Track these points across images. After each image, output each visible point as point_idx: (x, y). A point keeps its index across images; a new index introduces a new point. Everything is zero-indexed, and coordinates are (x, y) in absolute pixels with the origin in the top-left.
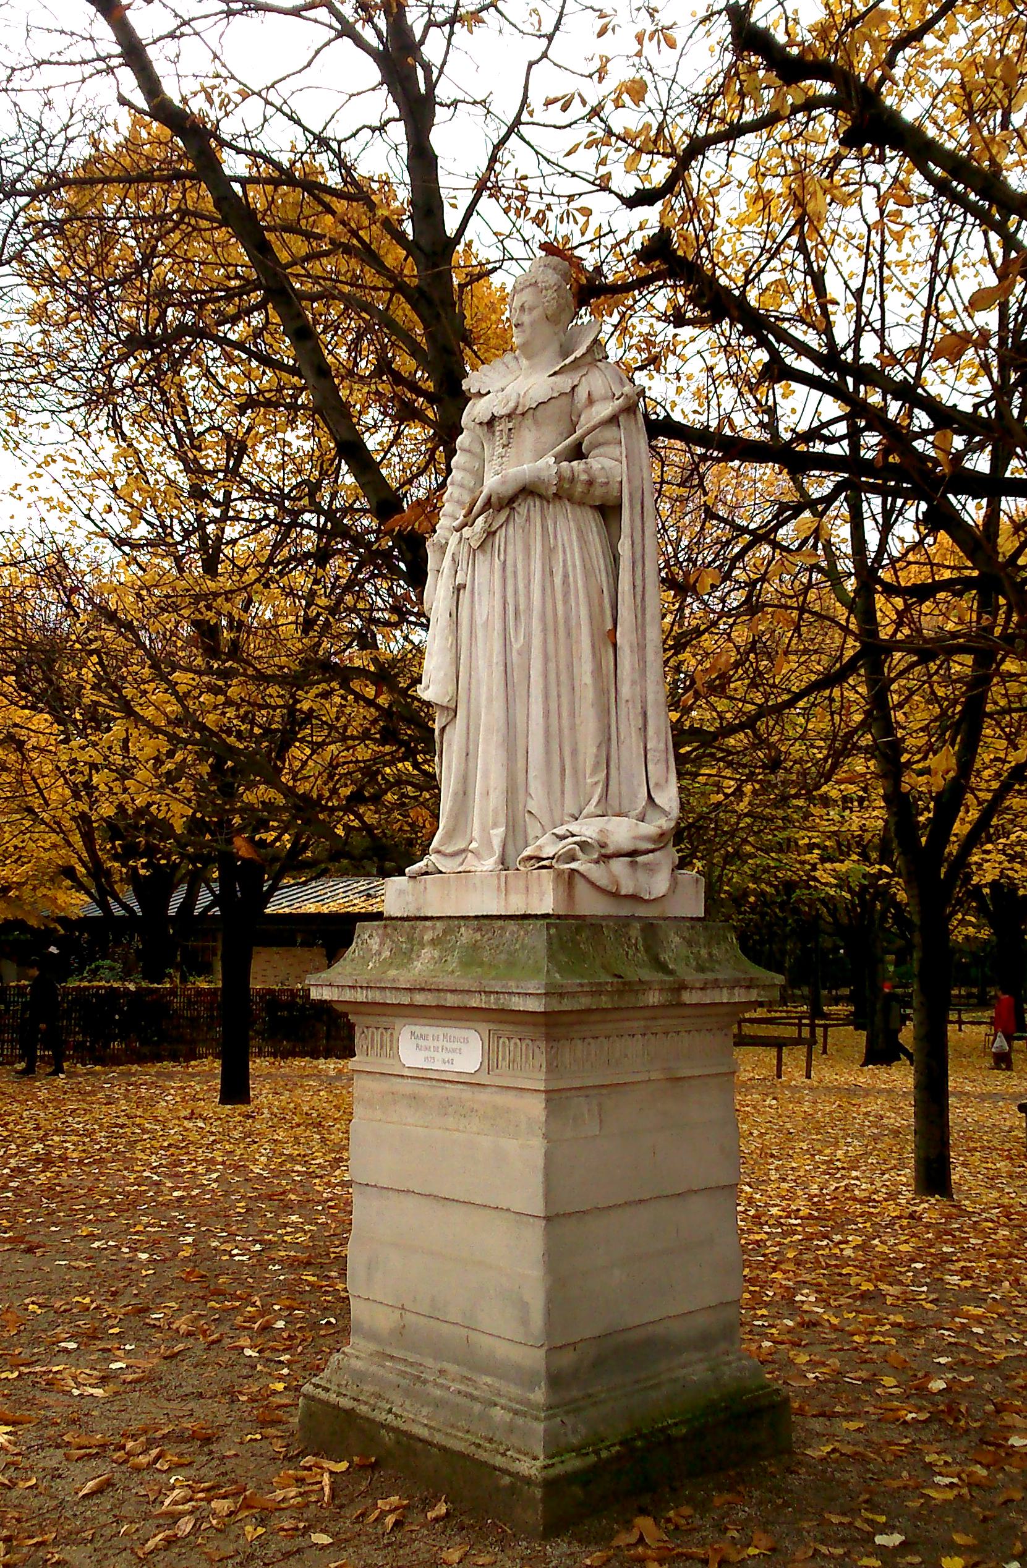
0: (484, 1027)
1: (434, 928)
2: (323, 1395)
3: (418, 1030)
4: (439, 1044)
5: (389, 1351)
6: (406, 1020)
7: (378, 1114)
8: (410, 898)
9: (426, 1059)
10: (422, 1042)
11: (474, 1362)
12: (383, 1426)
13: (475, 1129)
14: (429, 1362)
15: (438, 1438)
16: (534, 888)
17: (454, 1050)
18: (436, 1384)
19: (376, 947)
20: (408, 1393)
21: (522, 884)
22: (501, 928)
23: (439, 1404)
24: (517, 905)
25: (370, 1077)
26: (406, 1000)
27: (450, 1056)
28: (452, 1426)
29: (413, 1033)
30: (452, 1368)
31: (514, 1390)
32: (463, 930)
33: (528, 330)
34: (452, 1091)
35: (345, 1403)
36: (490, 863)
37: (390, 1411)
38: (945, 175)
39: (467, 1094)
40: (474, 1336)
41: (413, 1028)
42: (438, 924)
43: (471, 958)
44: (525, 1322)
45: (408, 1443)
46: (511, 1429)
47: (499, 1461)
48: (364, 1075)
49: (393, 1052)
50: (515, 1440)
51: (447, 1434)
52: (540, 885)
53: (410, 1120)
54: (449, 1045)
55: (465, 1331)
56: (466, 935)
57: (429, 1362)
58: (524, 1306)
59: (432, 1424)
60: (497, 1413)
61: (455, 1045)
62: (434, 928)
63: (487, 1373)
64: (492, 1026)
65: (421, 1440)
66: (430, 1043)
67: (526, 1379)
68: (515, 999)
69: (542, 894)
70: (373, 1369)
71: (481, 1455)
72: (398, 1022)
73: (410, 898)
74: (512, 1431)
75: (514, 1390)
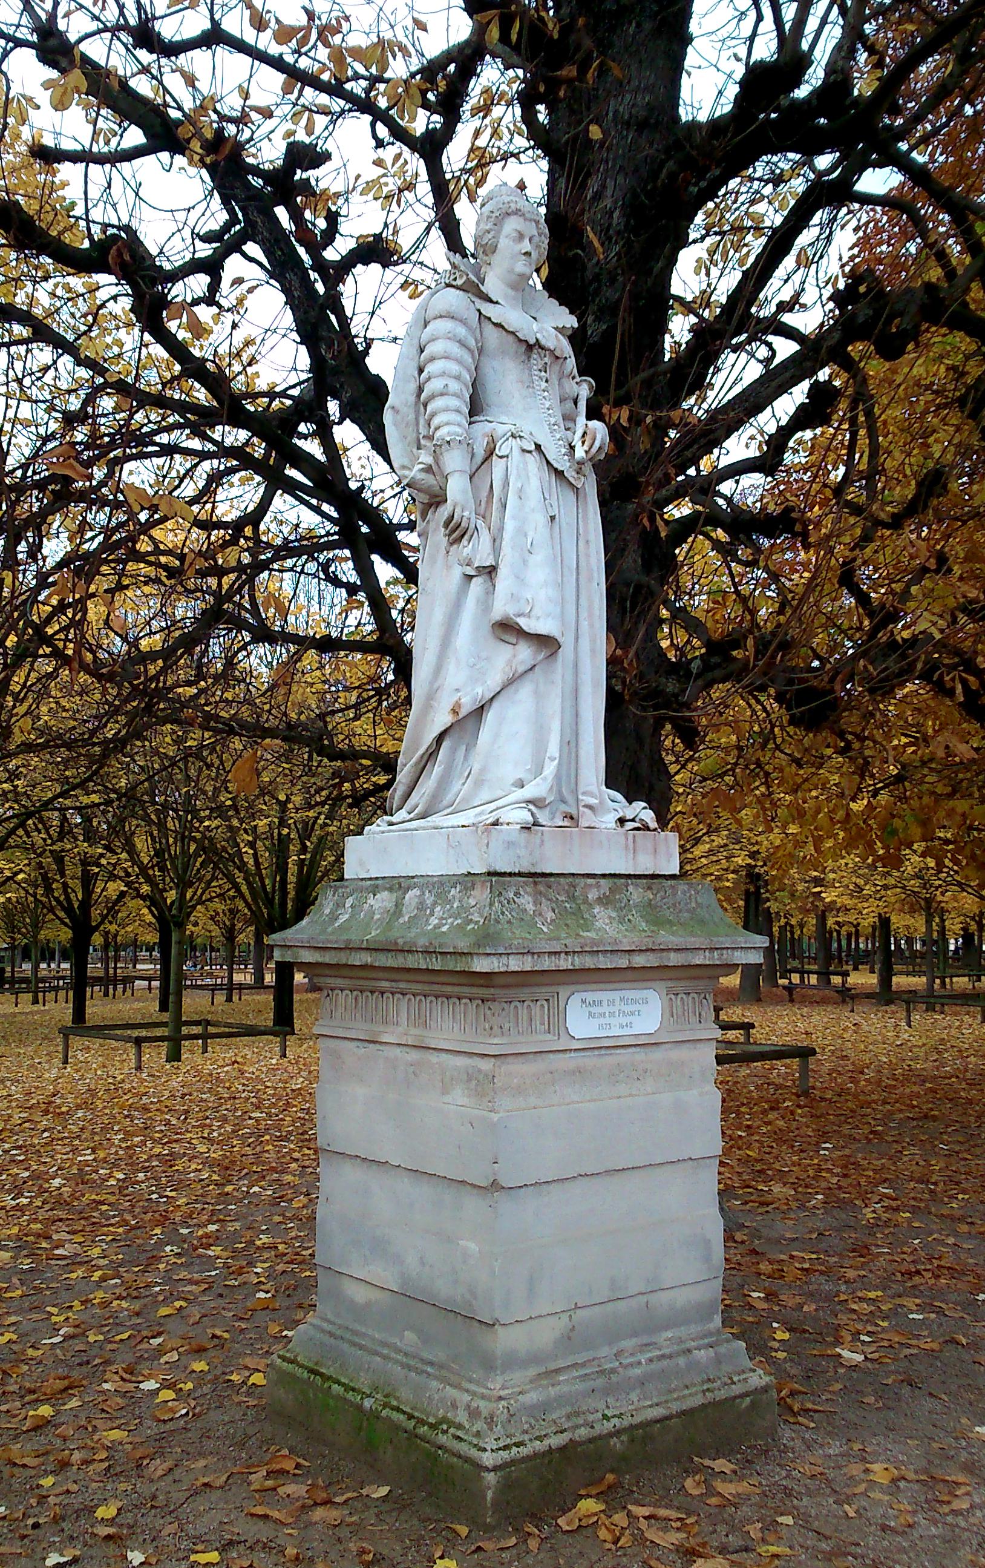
0: (662, 986)
1: (598, 886)
2: (524, 1451)
3: (590, 996)
4: (615, 1009)
5: (552, 1366)
6: (573, 988)
7: (533, 1101)
8: (522, 852)
9: (601, 1026)
10: (593, 1010)
11: (650, 1324)
12: (611, 1435)
13: (649, 1090)
14: (605, 1351)
15: (675, 1407)
16: (662, 849)
17: (632, 1013)
18: (626, 1367)
19: (530, 907)
20: (607, 1391)
21: (650, 845)
22: (672, 887)
23: (642, 1383)
24: (645, 865)
25: (521, 1059)
26: (623, 962)
27: (629, 1019)
28: (670, 1392)
29: (583, 1001)
30: (628, 1344)
31: (694, 1329)
32: (631, 888)
34: (623, 1056)
35: (556, 1441)
37: (605, 1417)
38: (805, 385)
39: (639, 1055)
40: (653, 1298)
41: (584, 995)
42: (602, 881)
43: (653, 914)
44: (707, 1259)
45: (642, 1435)
46: (718, 1360)
47: (737, 1390)
48: (510, 1059)
49: (557, 1023)
50: (726, 1368)
51: (676, 1399)
52: (668, 847)
53: (576, 1098)
54: (628, 1009)
55: (643, 1299)
56: (636, 893)
57: (605, 1351)
58: (707, 1242)
59: (655, 1400)
60: (702, 1355)
61: (637, 1007)
62: (598, 886)
63: (667, 1328)
64: (670, 984)
65: (658, 1421)
66: (605, 1009)
67: (702, 1312)
68: (737, 954)
69: (670, 855)
70: (552, 1391)
71: (722, 1394)
72: (564, 992)
73: (522, 852)
74: (720, 1362)
75: (694, 1329)
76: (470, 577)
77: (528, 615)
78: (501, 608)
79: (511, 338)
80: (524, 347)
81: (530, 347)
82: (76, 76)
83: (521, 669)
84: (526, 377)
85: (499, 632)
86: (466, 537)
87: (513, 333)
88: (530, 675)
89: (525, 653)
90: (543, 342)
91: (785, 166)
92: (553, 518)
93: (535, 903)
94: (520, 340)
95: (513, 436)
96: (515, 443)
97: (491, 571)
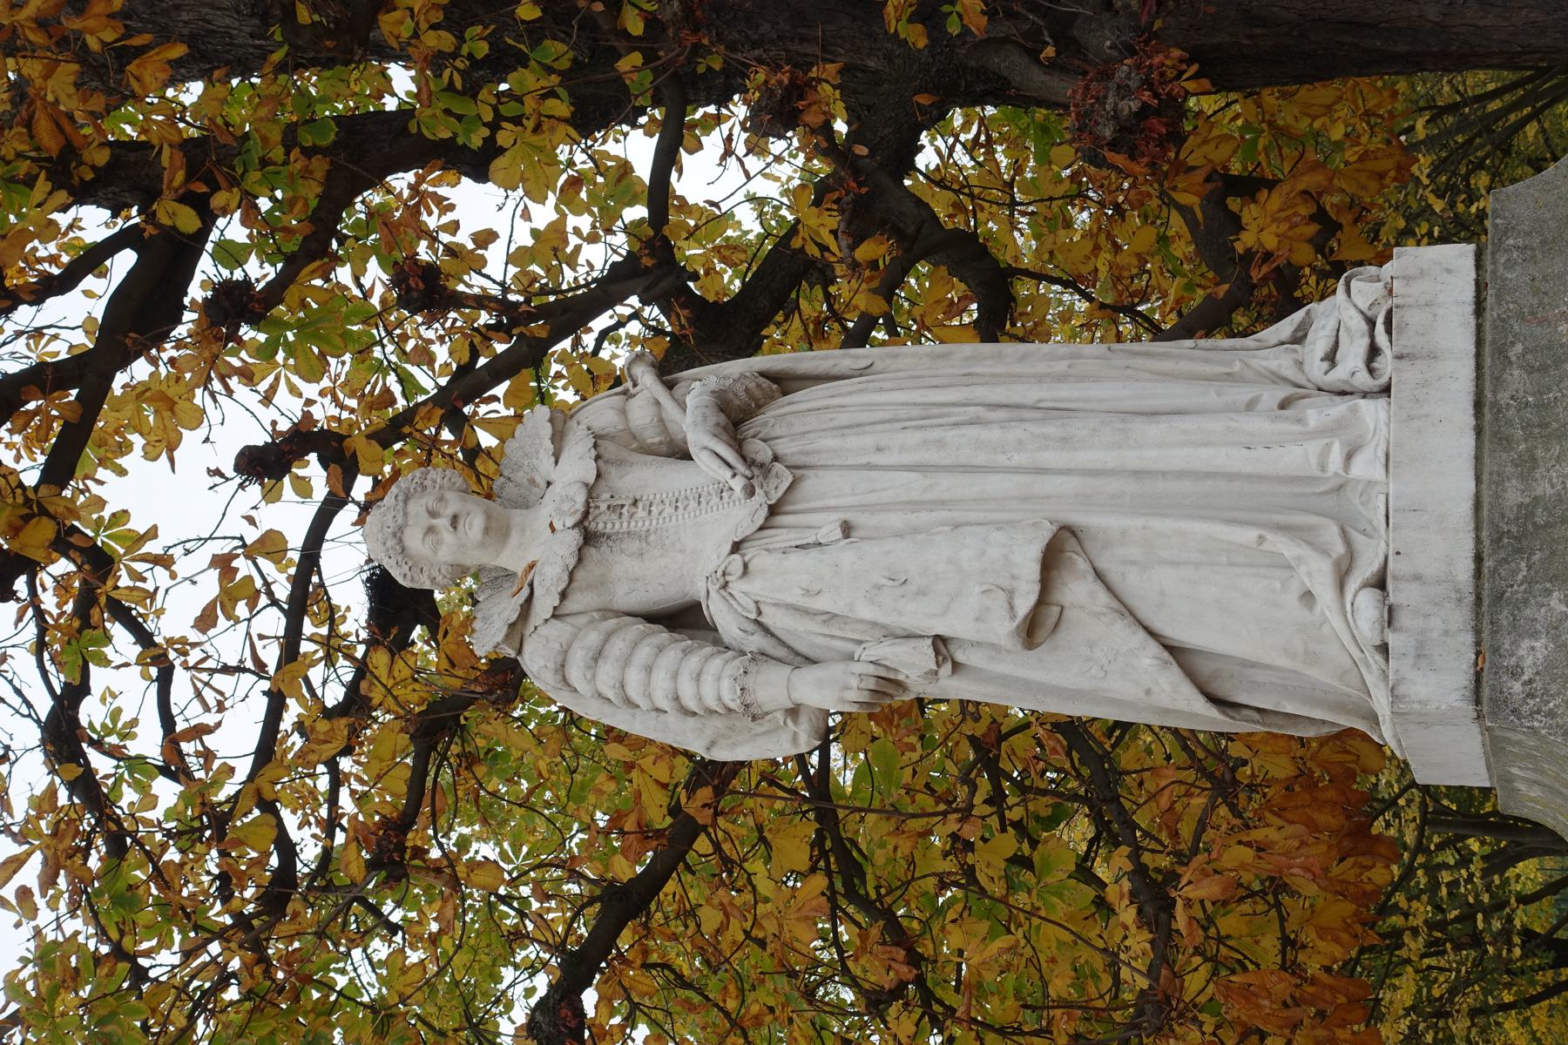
24: (1455, 334)
33: (470, 506)
36: (1372, 412)
76: (956, 666)
77: (1010, 594)
78: (1003, 629)
79: (579, 575)
80: (591, 552)
81: (589, 538)
82: (666, 231)
83: (1103, 597)
84: (634, 545)
85: (1041, 633)
86: (891, 676)
87: (571, 574)
88: (1114, 578)
89: (1077, 590)
90: (578, 517)
91: (46, 265)
92: (847, 529)
93: (1535, 635)
94: (580, 560)
95: (725, 586)
96: (736, 587)
97: (940, 643)
